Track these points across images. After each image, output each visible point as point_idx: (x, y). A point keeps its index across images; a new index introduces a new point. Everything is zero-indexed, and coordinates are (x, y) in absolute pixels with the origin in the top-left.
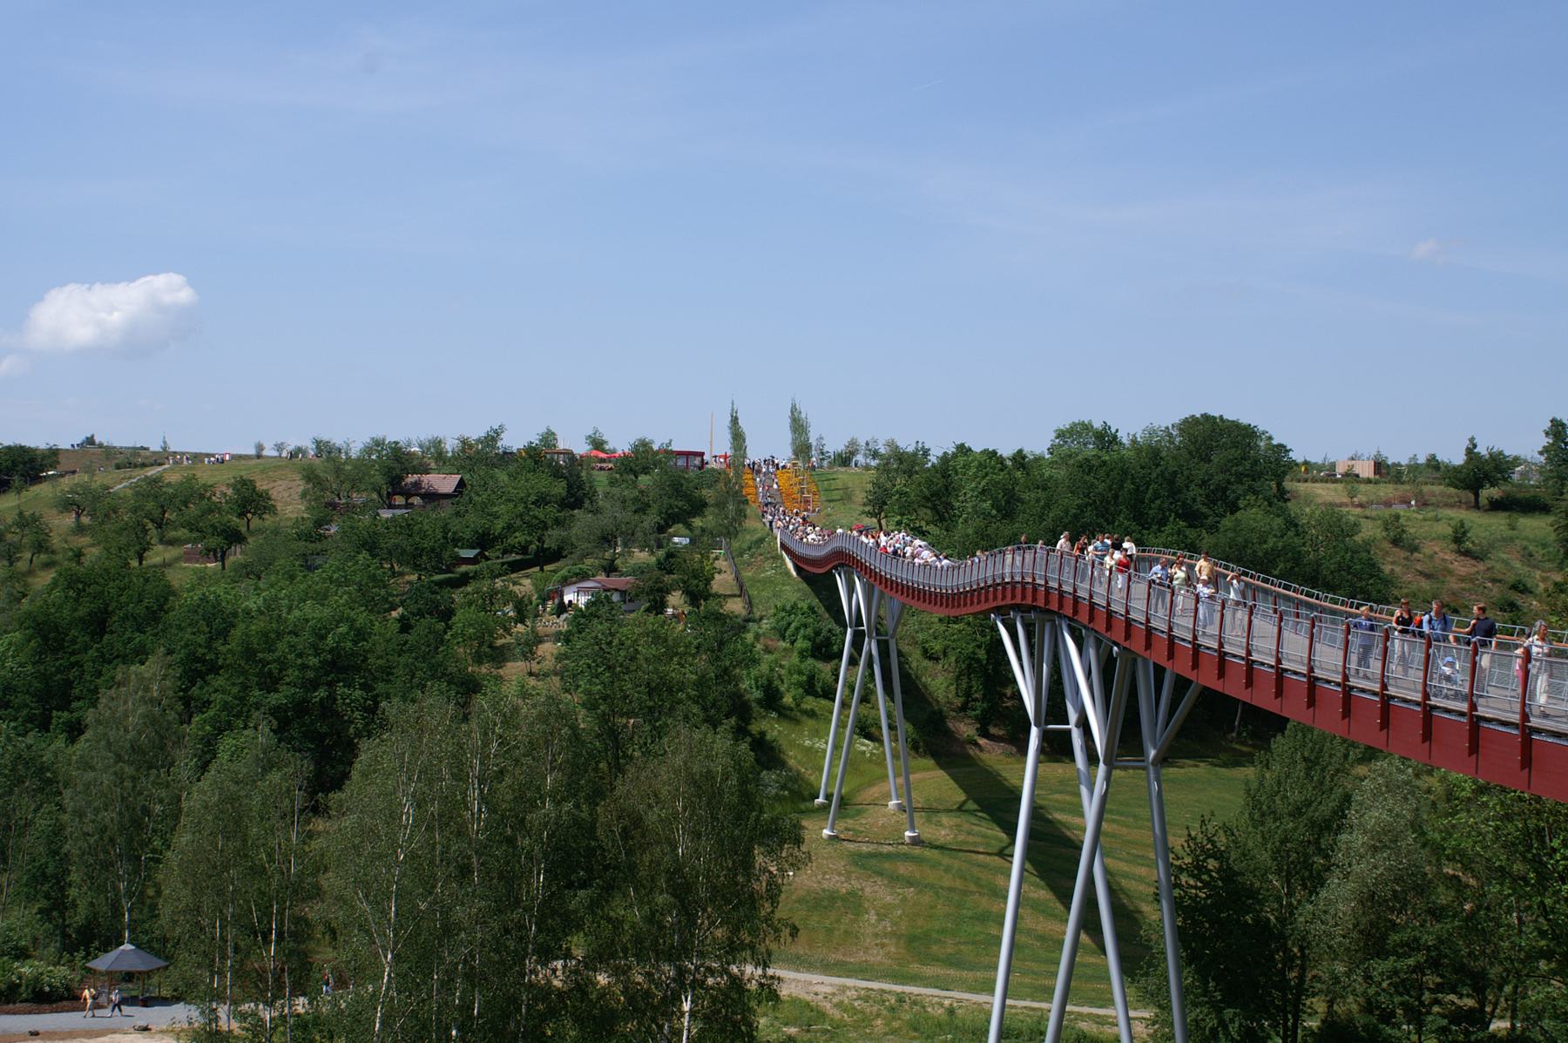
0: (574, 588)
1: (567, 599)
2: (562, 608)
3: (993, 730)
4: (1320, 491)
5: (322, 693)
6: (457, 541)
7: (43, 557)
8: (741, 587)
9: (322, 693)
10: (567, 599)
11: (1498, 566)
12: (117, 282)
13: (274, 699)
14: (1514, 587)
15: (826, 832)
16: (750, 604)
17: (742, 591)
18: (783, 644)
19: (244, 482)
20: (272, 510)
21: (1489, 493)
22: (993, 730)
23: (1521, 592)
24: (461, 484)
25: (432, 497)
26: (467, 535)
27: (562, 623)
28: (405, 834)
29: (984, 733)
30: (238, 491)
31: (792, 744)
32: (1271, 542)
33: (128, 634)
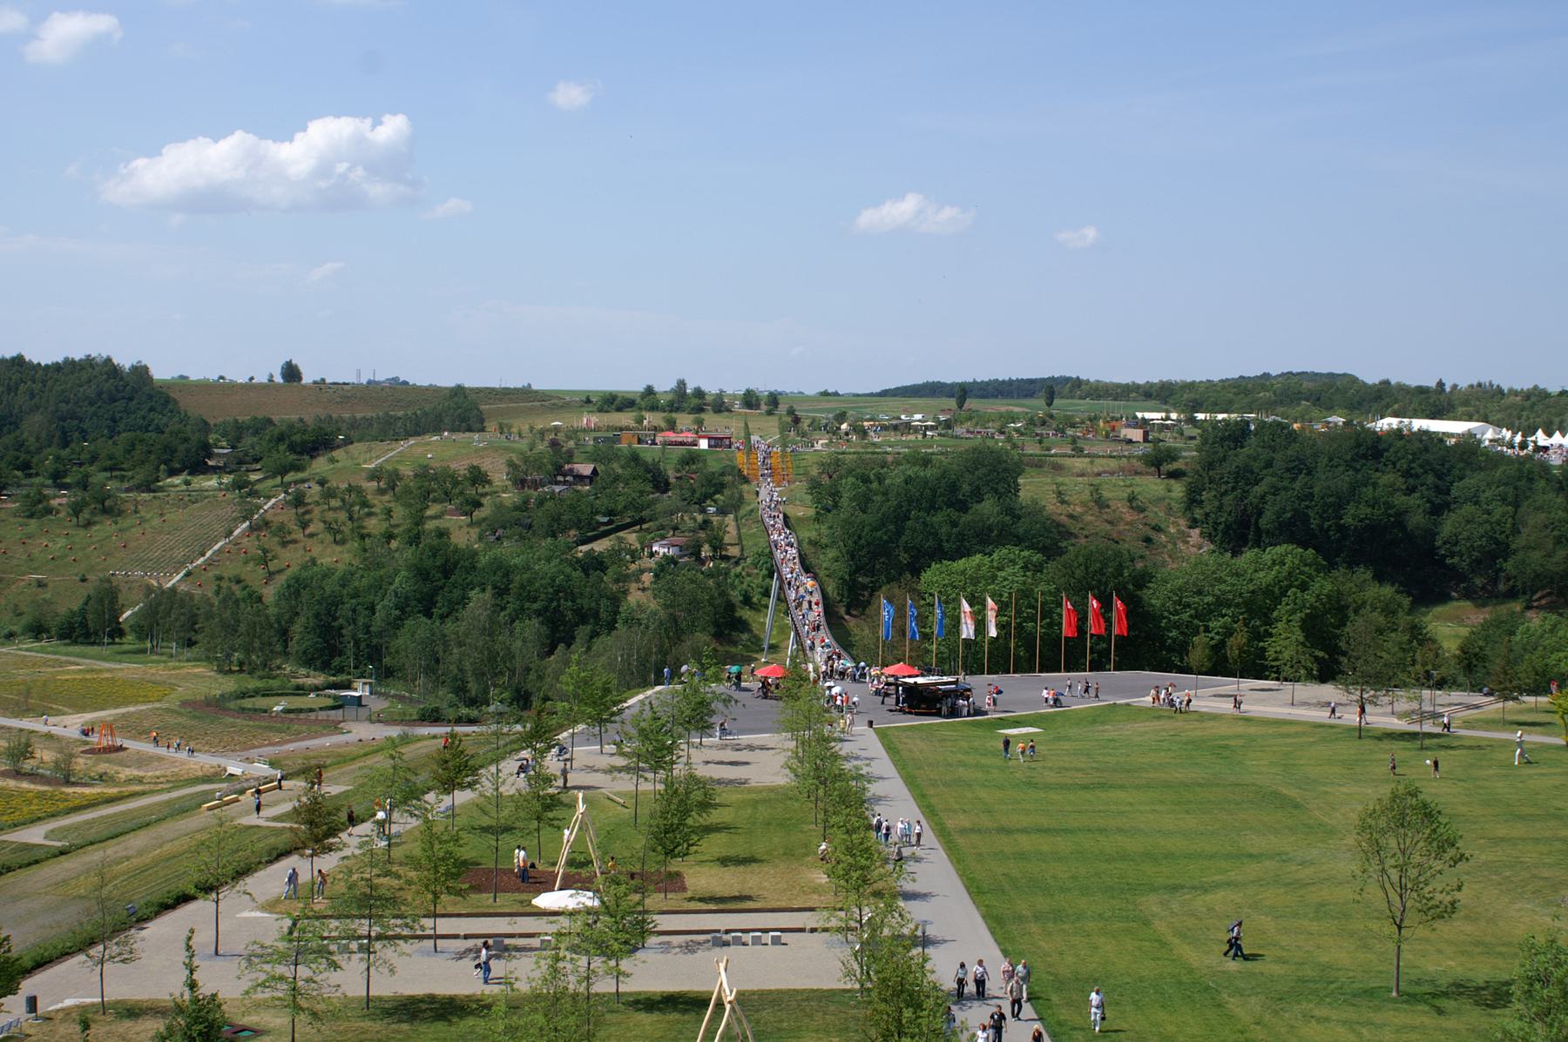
0: (657, 544)
1: (654, 549)
2: (652, 555)
3: (854, 612)
4: (1077, 464)
5: (555, 604)
6: (597, 513)
7: (366, 510)
8: (740, 538)
9: (555, 604)
10: (654, 549)
11: (1151, 515)
12: (427, 389)
13: (535, 606)
14: (1153, 528)
15: (763, 660)
16: (742, 550)
17: (740, 542)
18: (756, 571)
19: (474, 467)
20: (489, 482)
21: (1166, 467)
22: (854, 612)
23: (1157, 531)
24: (595, 471)
25: (580, 478)
26: (603, 509)
27: (652, 563)
28: (1510, 794)
29: (848, 613)
30: (471, 473)
31: (755, 621)
32: (991, 520)
33: (464, 576)
